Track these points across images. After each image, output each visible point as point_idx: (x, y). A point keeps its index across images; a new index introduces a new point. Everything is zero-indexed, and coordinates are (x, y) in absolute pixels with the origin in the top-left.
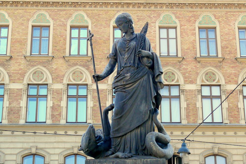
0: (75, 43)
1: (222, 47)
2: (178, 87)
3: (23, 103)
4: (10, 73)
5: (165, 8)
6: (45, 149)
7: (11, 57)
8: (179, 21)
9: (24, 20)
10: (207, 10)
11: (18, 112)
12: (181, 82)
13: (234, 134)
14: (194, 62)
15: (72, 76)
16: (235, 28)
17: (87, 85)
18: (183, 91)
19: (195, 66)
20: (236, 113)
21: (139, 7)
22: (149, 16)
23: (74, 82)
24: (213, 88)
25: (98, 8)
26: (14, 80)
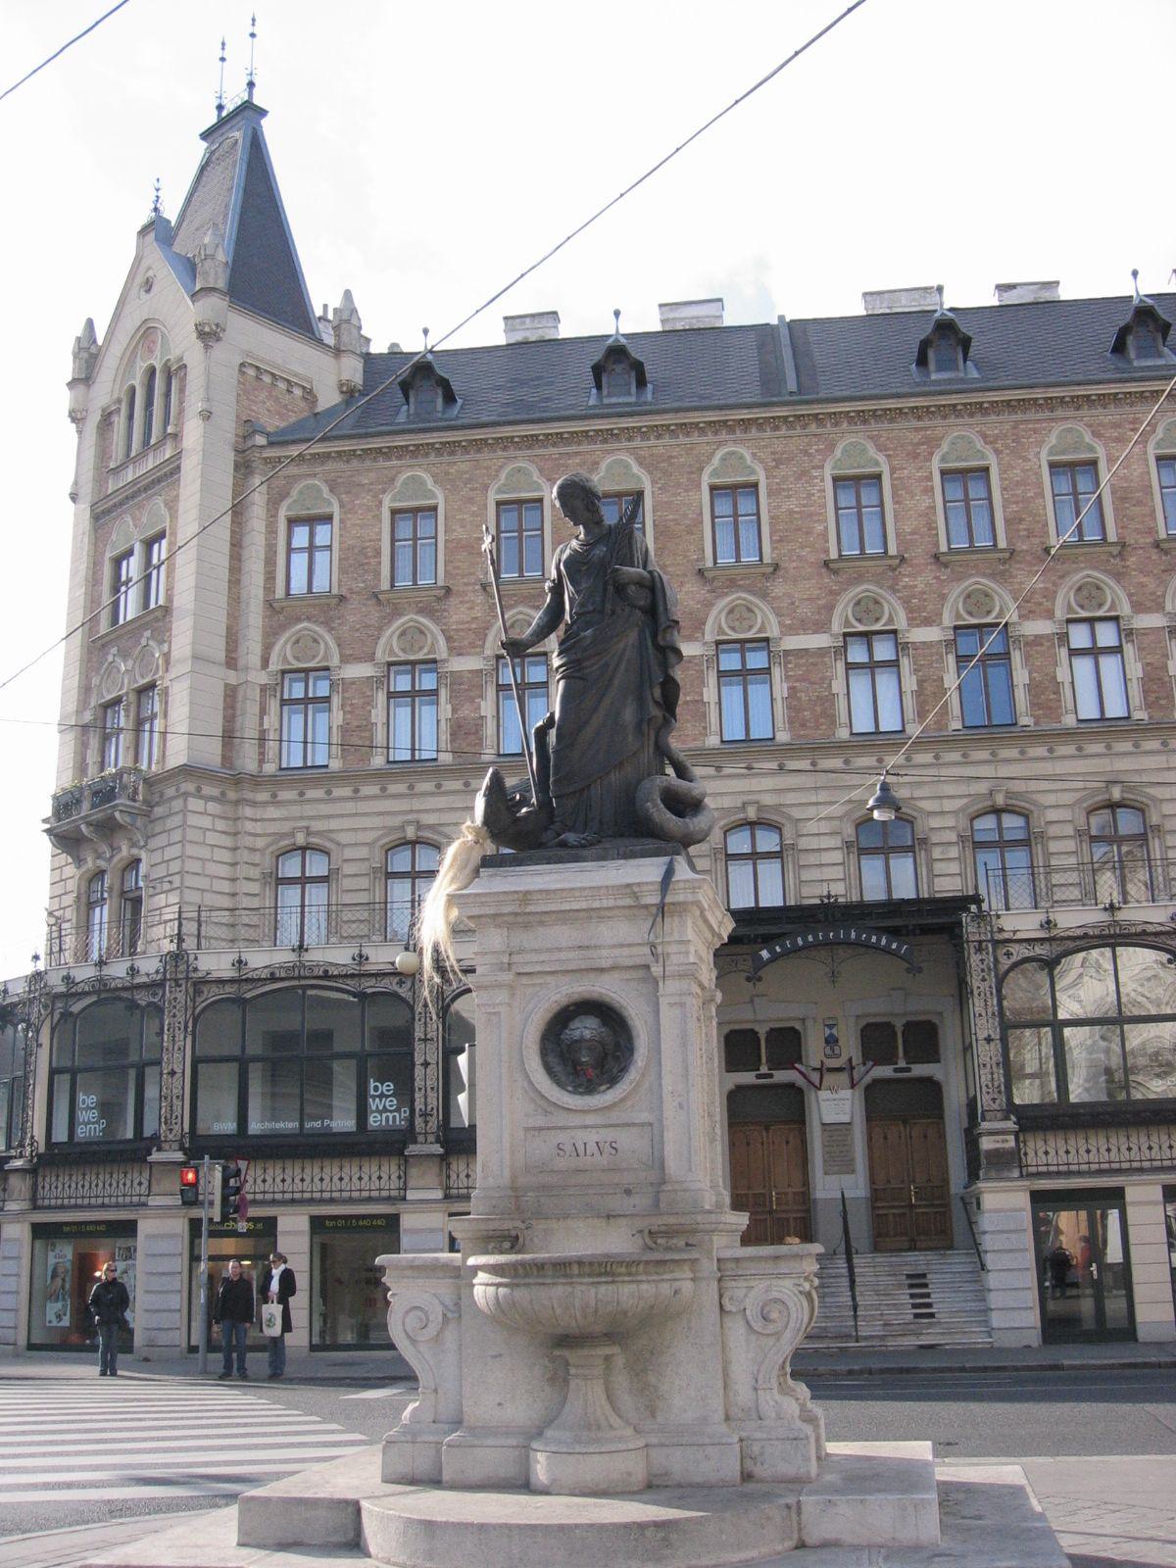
0: (299, 562)
1: (1007, 521)
2: (892, 635)
3: (487, 708)
4: (448, 630)
5: (845, 424)
6: (1147, 790)
7: (448, 590)
8: (888, 456)
9: (476, 489)
10: (959, 421)
11: (477, 732)
12: (901, 622)
13: (1046, 754)
14: (934, 567)
15: (727, 617)
16: (1040, 466)
17: (767, 640)
18: (1130, 633)
19: (936, 578)
20: (1052, 696)
21: (777, 428)
22: (806, 453)
23: (403, 657)
24: (1100, 628)
25: (667, 440)
26: (461, 648)
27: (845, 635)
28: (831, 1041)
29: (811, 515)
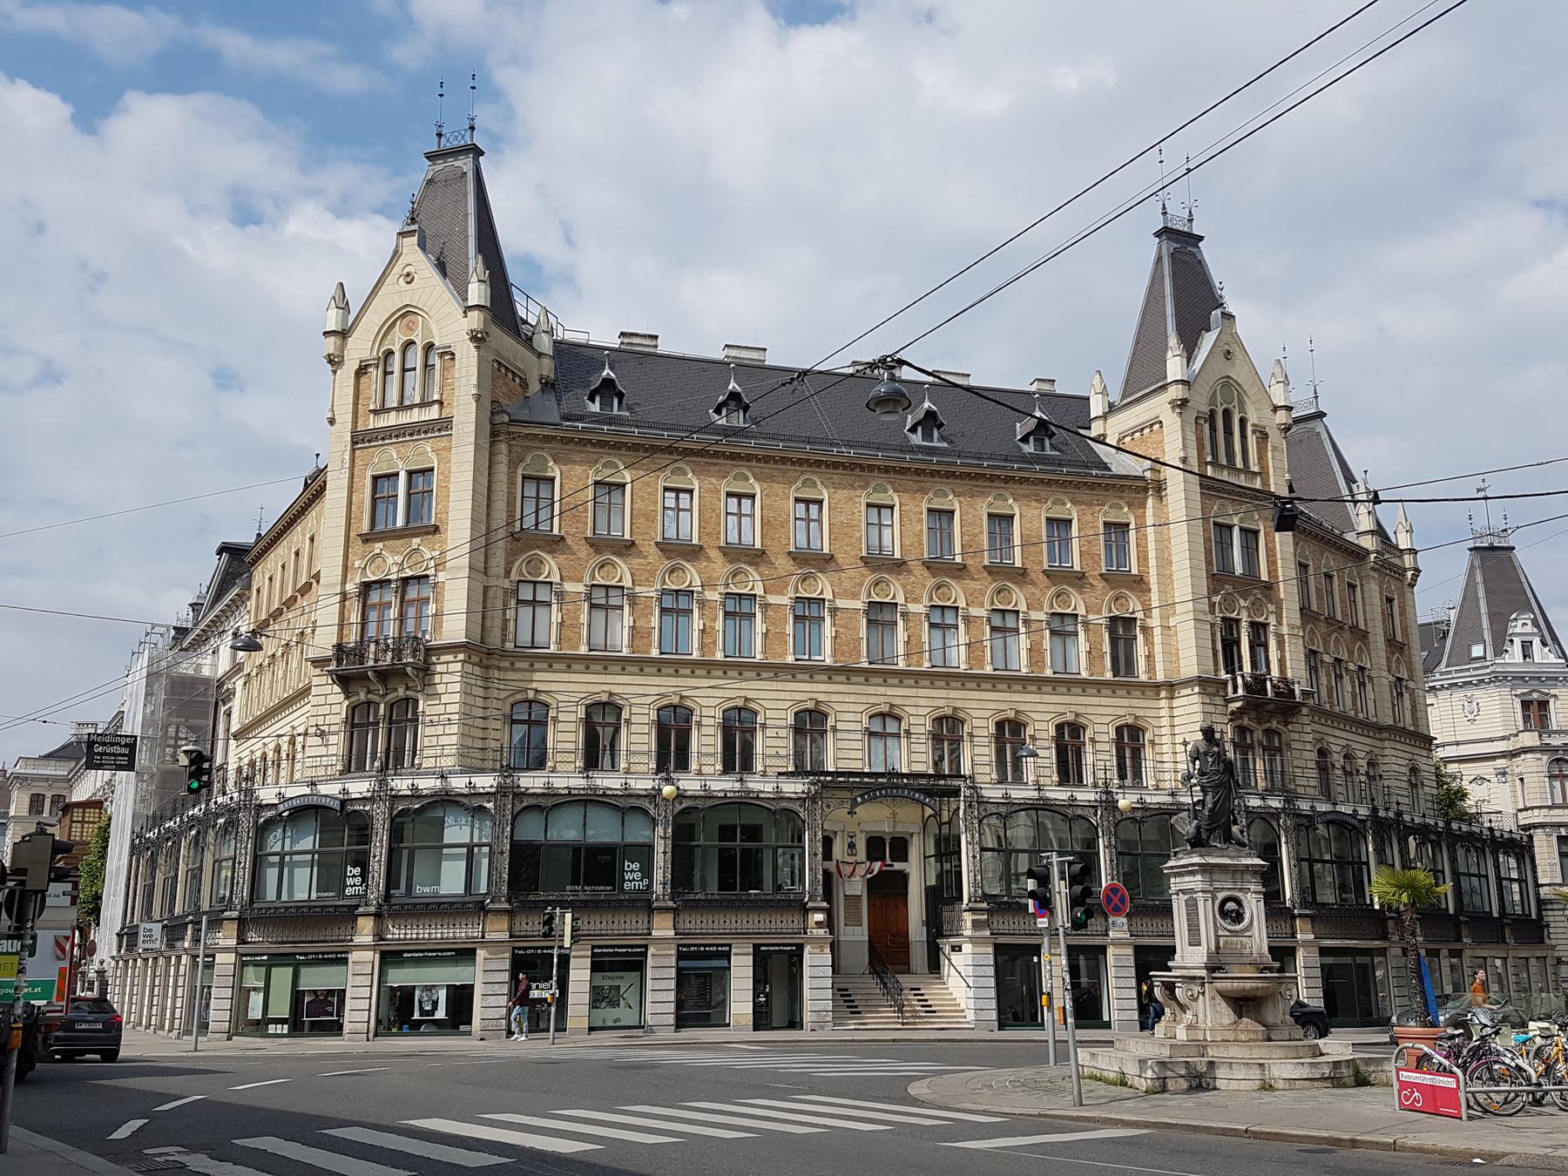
3: (655, 622)
27: (519, 581)
28: (852, 846)
29: (853, 526)
